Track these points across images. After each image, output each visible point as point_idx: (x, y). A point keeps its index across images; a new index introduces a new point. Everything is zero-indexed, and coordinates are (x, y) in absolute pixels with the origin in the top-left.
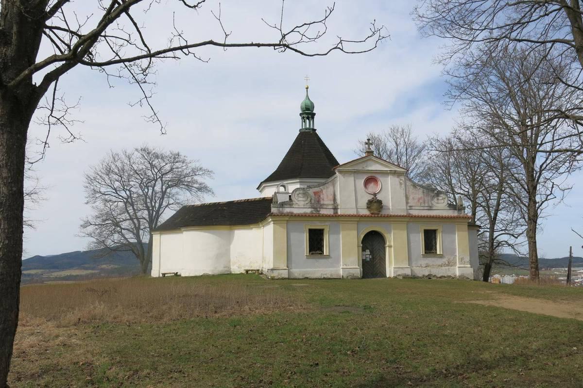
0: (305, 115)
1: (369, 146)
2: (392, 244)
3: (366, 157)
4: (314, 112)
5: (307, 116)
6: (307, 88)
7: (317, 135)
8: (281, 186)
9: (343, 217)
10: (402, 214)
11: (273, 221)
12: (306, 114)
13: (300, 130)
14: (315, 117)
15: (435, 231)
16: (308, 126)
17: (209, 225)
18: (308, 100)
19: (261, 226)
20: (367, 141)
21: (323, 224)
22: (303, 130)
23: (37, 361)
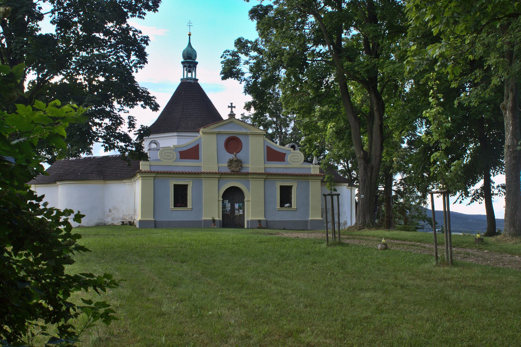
0: (186, 64)
1: (232, 109)
2: (250, 199)
3: (228, 119)
4: (196, 60)
5: (188, 65)
6: (190, 35)
7: (198, 85)
8: (154, 143)
9: (205, 174)
10: (260, 172)
11: (142, 177)
12: (188, 63)
13: (181, 79)
14: (197, 66)
15: (290, 187)
16: (194, 77)
17: (88, 179)
18: (190, 48)
19: (133, 180)
20: (230, 105)
21: (187, 181)
22: (185, 81)
23: (330, 279)
